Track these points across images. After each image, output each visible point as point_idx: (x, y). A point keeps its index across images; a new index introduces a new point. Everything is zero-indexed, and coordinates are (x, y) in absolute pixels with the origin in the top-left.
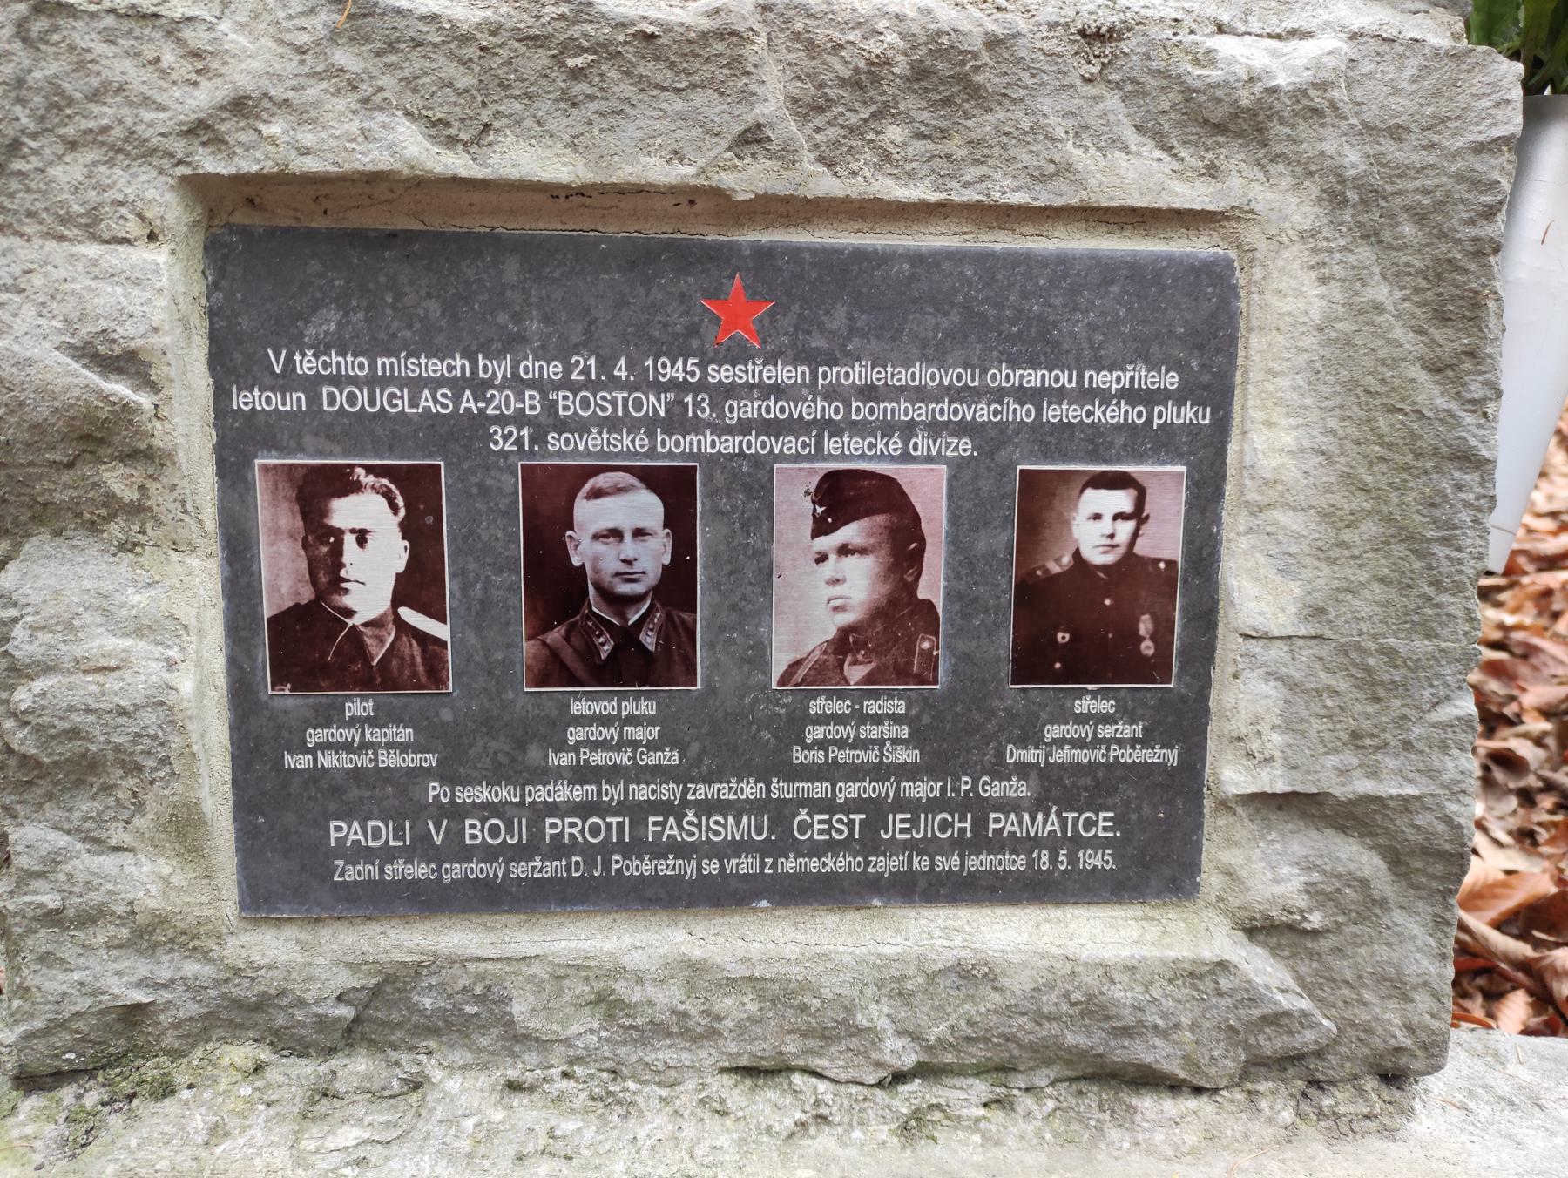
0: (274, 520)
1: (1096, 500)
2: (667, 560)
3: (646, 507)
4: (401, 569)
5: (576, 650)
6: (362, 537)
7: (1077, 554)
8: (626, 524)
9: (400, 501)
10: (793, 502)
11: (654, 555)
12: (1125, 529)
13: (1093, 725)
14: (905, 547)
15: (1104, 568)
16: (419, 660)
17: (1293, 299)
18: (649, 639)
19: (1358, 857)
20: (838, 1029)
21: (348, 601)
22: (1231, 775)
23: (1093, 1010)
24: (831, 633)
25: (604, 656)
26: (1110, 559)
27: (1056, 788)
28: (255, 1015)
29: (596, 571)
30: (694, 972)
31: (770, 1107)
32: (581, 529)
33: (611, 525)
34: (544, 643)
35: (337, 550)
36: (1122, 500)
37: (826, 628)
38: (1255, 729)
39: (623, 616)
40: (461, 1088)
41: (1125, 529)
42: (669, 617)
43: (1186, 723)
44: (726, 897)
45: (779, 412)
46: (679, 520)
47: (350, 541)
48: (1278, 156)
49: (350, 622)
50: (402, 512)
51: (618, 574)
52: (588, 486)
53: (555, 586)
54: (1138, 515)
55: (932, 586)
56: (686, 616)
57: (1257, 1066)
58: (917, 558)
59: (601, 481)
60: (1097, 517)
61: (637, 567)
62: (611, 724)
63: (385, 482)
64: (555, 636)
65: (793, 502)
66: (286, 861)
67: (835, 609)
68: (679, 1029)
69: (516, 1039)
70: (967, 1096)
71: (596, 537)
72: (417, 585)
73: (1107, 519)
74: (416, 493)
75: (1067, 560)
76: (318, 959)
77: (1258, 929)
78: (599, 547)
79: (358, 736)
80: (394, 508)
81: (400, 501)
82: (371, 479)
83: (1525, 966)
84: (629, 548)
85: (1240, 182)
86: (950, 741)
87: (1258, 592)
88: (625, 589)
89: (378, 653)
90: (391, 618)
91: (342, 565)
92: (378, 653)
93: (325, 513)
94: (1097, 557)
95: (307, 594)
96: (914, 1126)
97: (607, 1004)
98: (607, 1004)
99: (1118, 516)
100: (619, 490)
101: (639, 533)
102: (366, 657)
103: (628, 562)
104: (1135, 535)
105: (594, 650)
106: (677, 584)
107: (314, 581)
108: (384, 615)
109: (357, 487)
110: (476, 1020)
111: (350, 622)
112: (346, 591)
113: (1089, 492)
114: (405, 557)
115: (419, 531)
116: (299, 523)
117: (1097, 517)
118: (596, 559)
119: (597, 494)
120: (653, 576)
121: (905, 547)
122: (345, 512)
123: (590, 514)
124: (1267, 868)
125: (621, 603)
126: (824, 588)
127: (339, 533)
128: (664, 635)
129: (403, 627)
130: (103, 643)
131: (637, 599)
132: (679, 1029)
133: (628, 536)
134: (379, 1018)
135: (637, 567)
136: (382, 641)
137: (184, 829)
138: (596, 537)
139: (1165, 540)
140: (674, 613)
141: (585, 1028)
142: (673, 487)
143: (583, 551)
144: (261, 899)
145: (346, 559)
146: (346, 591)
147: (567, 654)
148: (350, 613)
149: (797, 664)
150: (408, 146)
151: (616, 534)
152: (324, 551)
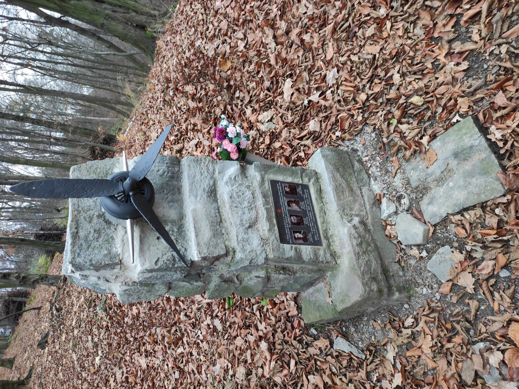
0: (298, 242)
10: (290, 208)
11: (295, 218)
13: (299, 190)
17: (273, 177)
19: (304, 174)
20: (321, 207)
22: (301, 182)
23: (317, 191)
27: (304, 193)
28: (329, 245)
30: (320, 217)
31: (327, 213)
38: (297, 180)
40: (330, 233)
43: (298, 185)
44: (315, 214)
45: (285, 209)
46: (293, 216)
55: (293, 200)
57: (318, 181)
62: (306, 221)
65: (290, 208)
66: (318, 243)
68: (324, 218)
69: (326, 230)
70: (324, 200)
72: (300, 233)
74: (295, 232)
76: (324, 242)
77: (309, 181)
79: (310, 237)
83: (293, 162)
85: (266, 179)
86: (302, 200)
87: (289, 180)
96: (327, 203)
97: (323, 223)
98: (323, 223)
106: (296, 216)
110: (326, 231)
115: (297, 232)
124: (306, 181)
126: (295, 207)
130: (308, 252)
132: (324, 218)
134: (327, 238)
137: (319, 249)
139: (287, 185)
141: (325, 225)
142: (291, 216)
144: (321, 245)
150: (276, 228)
152: (299, 238)
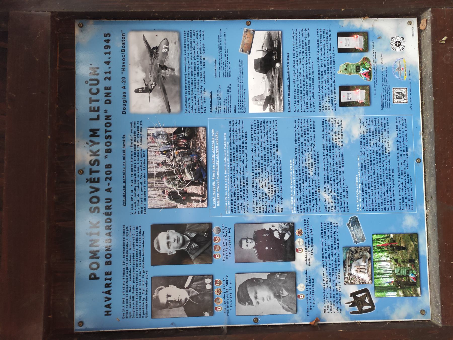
1: (244, 246)
2: (174, 231)
3: (162, 237)
4: (175, 287)
5: (196, 252)
6: (168, 296)
7: (254, 248)
8: (165, 241)
9: (160, 287)
11: (173, 235)
12: (249, 240)
14: (254, 282)
15: (255, 243)
16: (197, 283)
18: (193, 235)
21: (183, 299)
24: (276, 299)
25: (197, 246)
26: (254, 242)
29: (177, 248)
32: (167, 251)
33: (166, 244)
34: (194, 259)
35: (172, 301)
36: (244, 242)
37: (275, 301)
39: (188, 241)
41: (249, 240)
42: (188, 230)
47: (169, 299)
48: (243, 287)
49: (188, 299)
50: (163, 287)
51: (178, 243)
52: (157, 250)
53: (181, 257)
54: (247, 239)
56: (188, 226)
58: (257, 280)
59: (156, 246)
60: (247, 245)
61: (176, 238)
63: (156, 290)
64: (192, 257)
67: (270, 299)
71: (169, 248)
73: (247, 244)
75: (254, 250)
78: (171, 247)
80: (161, 289)
81: (160, 287)
82: (155, 294)
84: (171, 240)
88: (181, 241)
89: (196, 292)
90: (187, 289)
91: (175, 300)
92: (196, 292)
93: (163, 304)
94: (254, 244)
95: (182, 308)
99: (247, 242)
100: (158, 243)
101: (168, 238)
102: (197, 295)
103: (175, 240)
104: (250, 239)
105: (196, 248)
107: (178, 307)
108: (187, 291)
109: (157, 297)
111: (188, 299)
112: (181, 299)
113: (243, 247)
114: (173, 286)
116: (165, 310)
117: (247, 245)
118: (174, 248)
119: (159, 248)
120: (178, 234)
121: (254, 282)
122: (163, 300)
123: (164, 249)
125: (184, 242)
127: (168, 301)
128: (193, 232)
129: (189, 287)
131: (184, 238)
133: (169, 240)
135: (176, 238)
136: (193, 292)
138: (169, 248)
140: (187, 229)
143: (172, 251)
145: (174, 300)
146: (181, 299)
147: (197, 254)
148: (186, 299)
149: (283, 307)
151: (168, 243)
